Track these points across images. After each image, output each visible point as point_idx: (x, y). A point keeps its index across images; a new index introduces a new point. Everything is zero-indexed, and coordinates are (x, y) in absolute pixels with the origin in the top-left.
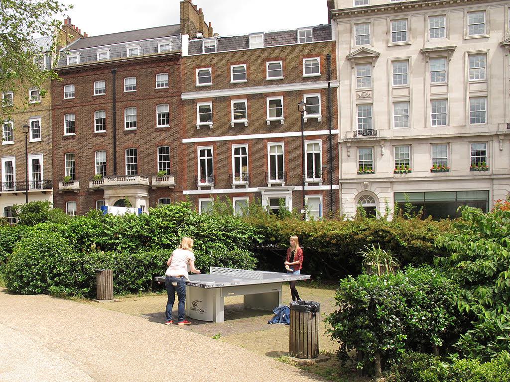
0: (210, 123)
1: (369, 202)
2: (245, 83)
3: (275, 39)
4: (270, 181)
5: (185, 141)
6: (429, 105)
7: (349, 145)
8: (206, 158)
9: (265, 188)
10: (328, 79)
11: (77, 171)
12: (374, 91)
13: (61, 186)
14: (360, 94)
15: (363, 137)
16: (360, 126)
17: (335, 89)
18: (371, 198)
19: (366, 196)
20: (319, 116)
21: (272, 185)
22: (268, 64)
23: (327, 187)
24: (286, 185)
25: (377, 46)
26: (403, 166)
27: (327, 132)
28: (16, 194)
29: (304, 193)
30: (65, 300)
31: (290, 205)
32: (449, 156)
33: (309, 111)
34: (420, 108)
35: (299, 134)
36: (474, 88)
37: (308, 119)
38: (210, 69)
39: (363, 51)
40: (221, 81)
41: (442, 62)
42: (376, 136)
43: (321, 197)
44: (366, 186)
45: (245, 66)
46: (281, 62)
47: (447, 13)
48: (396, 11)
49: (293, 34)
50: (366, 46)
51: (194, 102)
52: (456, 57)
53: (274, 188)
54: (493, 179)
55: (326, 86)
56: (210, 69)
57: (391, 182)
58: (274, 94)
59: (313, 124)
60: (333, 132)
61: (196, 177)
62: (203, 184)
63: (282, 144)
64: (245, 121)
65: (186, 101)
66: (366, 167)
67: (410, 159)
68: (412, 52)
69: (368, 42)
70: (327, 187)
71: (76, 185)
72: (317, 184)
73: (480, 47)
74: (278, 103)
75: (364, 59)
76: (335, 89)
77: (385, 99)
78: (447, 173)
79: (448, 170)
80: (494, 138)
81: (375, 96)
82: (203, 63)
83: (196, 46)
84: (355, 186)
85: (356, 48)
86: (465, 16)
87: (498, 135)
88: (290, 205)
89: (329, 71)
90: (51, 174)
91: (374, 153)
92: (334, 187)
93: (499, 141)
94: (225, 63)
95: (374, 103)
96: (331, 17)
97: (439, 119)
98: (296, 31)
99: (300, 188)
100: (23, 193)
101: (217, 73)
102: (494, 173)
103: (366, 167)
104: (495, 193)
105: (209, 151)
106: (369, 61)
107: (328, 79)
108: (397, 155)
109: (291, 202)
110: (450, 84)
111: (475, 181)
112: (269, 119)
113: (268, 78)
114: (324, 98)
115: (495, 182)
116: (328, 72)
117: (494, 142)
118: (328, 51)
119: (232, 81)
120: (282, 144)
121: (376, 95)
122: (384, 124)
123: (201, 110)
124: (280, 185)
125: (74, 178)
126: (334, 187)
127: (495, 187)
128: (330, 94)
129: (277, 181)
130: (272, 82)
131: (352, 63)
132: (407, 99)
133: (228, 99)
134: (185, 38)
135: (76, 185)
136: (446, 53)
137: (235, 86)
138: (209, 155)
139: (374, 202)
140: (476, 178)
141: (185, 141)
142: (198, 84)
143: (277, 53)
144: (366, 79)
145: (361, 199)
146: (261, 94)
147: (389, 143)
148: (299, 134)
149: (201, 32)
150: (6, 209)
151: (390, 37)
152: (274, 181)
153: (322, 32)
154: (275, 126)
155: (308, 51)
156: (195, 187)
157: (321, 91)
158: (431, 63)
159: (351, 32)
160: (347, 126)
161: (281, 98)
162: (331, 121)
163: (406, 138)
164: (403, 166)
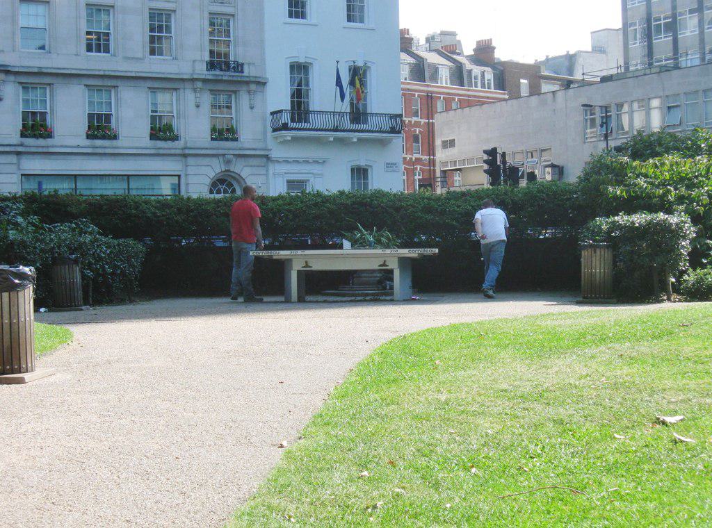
7: (199, 84)
15: (222, 73)
30: (426, 328)
32: (117, 111)
42: (243, 75)
57: (19, 153)
67: (48, 110)
78: (114, 143)
79: (115, 137)
80: (188, 85)
84: (206, 161)
87: (193, 80)
91: (117, 100)
93: (195, 90)
97: (156, 44)
102: (189, 145)
104: (192, 180)
108: (26, 102)
111: (94, 157)
115: (191, 161)
117: (187, 91)
127: (191, 170)
140: (161, 152)
147: (12, 78)
163: (44, 70)
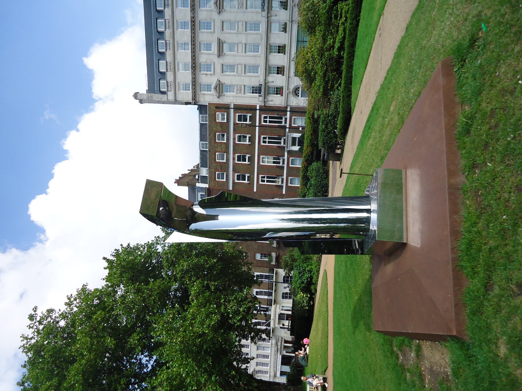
0: (247, 175)
1: (299, 91)
2: (227, 134)
3: (204, 136)
4: (282, 144)
5: (255, 190)
6: (248, 53)
8: (266, 179)
9: (286, 148)
10: (229, 108)
11: (266, 253)
12: (238, 84)
13: (273, 263)
14: (238, 92)
16: (256, 93)
17: (234, 105)
18: (297, 89)
19: (295, 92)
20: (249, 115)
21: (284, 144)
22: (217, 141)
23: (288, 113)
24: (285, 136)
25: (213, 81)
26: (280, 70)
27: (258, 112)
28: (275, 291)
29: (291, 127)
31: (297, 135)
33: (245, 120)
34: (250, 59)
35: (257, 128)
36: (240, 50)
37: (250, 121)
38: (217, 173)
39: (216, 88)
40: (224, 167)
41: (225, 45)
43: (294, 117)
44: (295, 5)
45: (217, 153)
46: (217, 134)
47: (199, 19)
48: (195, 69)
49: (202, 125)
50: (213, 87)
51: (234, 183)
52: (222, 38)
53: (286, 143)
54: (292, 21)
55: (232, 110)
56: (217, 173)
57: (289, 77)
58: (234, 139)
59: (253, 119)
60: (258, 108)
61: (278, 147)
62: (283, 122)
63: (261, 156)
64: (248, 136)
65: (233, 188)
66: (279, 91)
68: (218, 62)
69: (211, 85)
70: (288, 113)
71: (274, 255)
72: (286, 119)
73: (218, 24)
74: (240, 137)
75: (220, 88)
76: (234, 105)
77: (243, 78)
81: (241, 83)
82: (213, 176)
83: (204, 179)
85: (213, 92)
86: (202, 32)
87: (268, 17)
88: (297, 135)
89: (225, 108)
90: (266, 269)
92: (289, 109)
93: (271, 16)
94: (214, 164)
95: (245, 84)
96: (195, 104)
98: (201, 151)
99: (287, 130)
100: (275, 285)
101: (220, 169)
103: (279, 91)
105: (262, 177)
106: (221, 85)
107: (229, 108)
109: (294, 134)
110: (238, 42)
112: (247, 143)
113: (225, 141)
114: (239, 111)
116: (225, 108)
118: (213, 108)
119: (225, 180)
120: (261, 156)
121: (240, 83)
122: (257, 79)
123: (239, 140)
124: (285, 140)
125: (270, 255)
126: (289, 109)
128: (238, 108)
129: (282, 141)
130: (228, 139)
131: (221, 95)
132: (243, 66)
133: (234, 165)
134: (198, 185)
135: (274, 255)
136: (220, 44)
137: (228, 159)
138: (264, 177)
139: (299, 88)
141: (255, 190)
142: (225, 180)
143: (212, 135)
144: (230, 88)
145: (296, 95)
146: (234, 146)
148: (257, 128)
149: (195, 176)
150: (283, 298)
151: (208, 73)
152: (282, 143)
153: (202, 109)
154: (251, 159)
155: (213, 117)
156: (282, 168)
157: (235, 113)
158: (225, 51)
159: (204, 94)
160: (256, 100)
161: (237, 155)
162: (252, 109)
164: (280, 70)
